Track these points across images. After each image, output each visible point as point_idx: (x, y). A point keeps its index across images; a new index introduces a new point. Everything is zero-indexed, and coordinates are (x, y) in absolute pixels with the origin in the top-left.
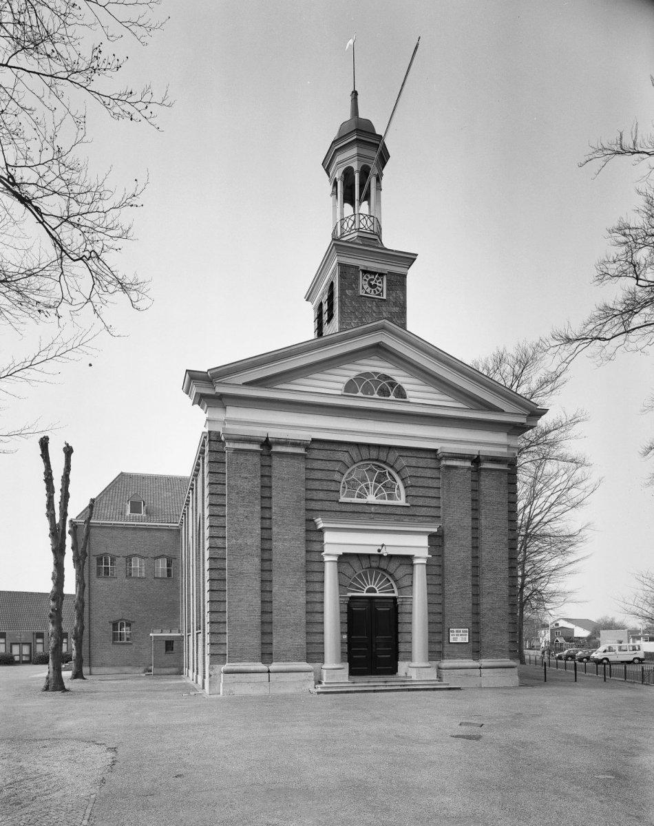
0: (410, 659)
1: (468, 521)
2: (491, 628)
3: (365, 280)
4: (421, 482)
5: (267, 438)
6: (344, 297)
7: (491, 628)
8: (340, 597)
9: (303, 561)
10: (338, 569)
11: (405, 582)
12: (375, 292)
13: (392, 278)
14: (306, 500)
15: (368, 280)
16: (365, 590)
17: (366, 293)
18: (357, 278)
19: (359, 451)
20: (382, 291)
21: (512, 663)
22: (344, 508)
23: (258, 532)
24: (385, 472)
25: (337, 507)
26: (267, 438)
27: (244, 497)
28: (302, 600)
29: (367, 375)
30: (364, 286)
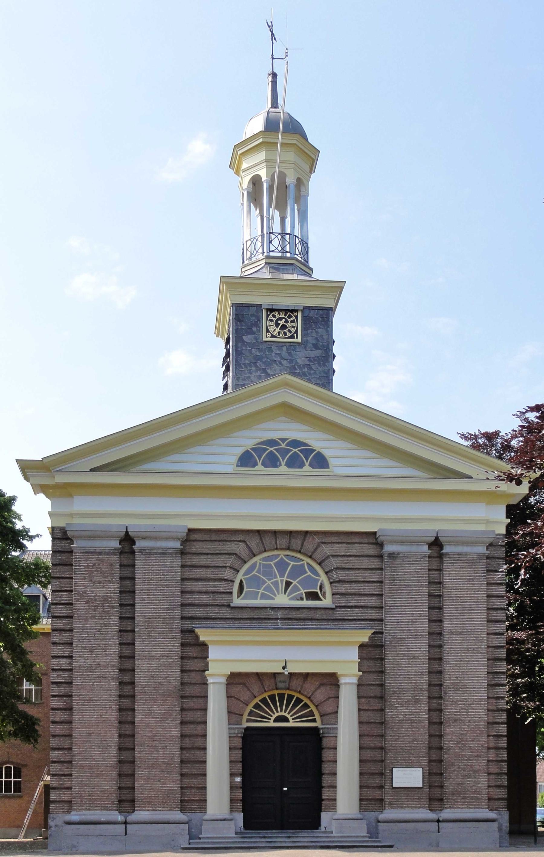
0: (334, 808)
1: (423, 625)
2: (459, 767)
3: (271, 320)
4: (353, 575)
5: (127, 532)
6: (240, 345)
7: (459, 767)
8: (229, 728)
9: (178, 683)
10: (227, 692)
11: (328, 708)
12: (285, 334)
13: (307, 312)
14: (182, 605)
15: (275, 319)
16: (274, 716)
17: (273, 336)
18: (259, 320)
19: (261, 539)
20: (296, 332)
21: (492, 815)
22: (237, 614)
23: (117, 648)
24: (304, 564)
25: (226, 612)
26: (127, 532)
27: (96, 606)
28: (176, 732)
29: (272, 442)
30: (270, 328)
